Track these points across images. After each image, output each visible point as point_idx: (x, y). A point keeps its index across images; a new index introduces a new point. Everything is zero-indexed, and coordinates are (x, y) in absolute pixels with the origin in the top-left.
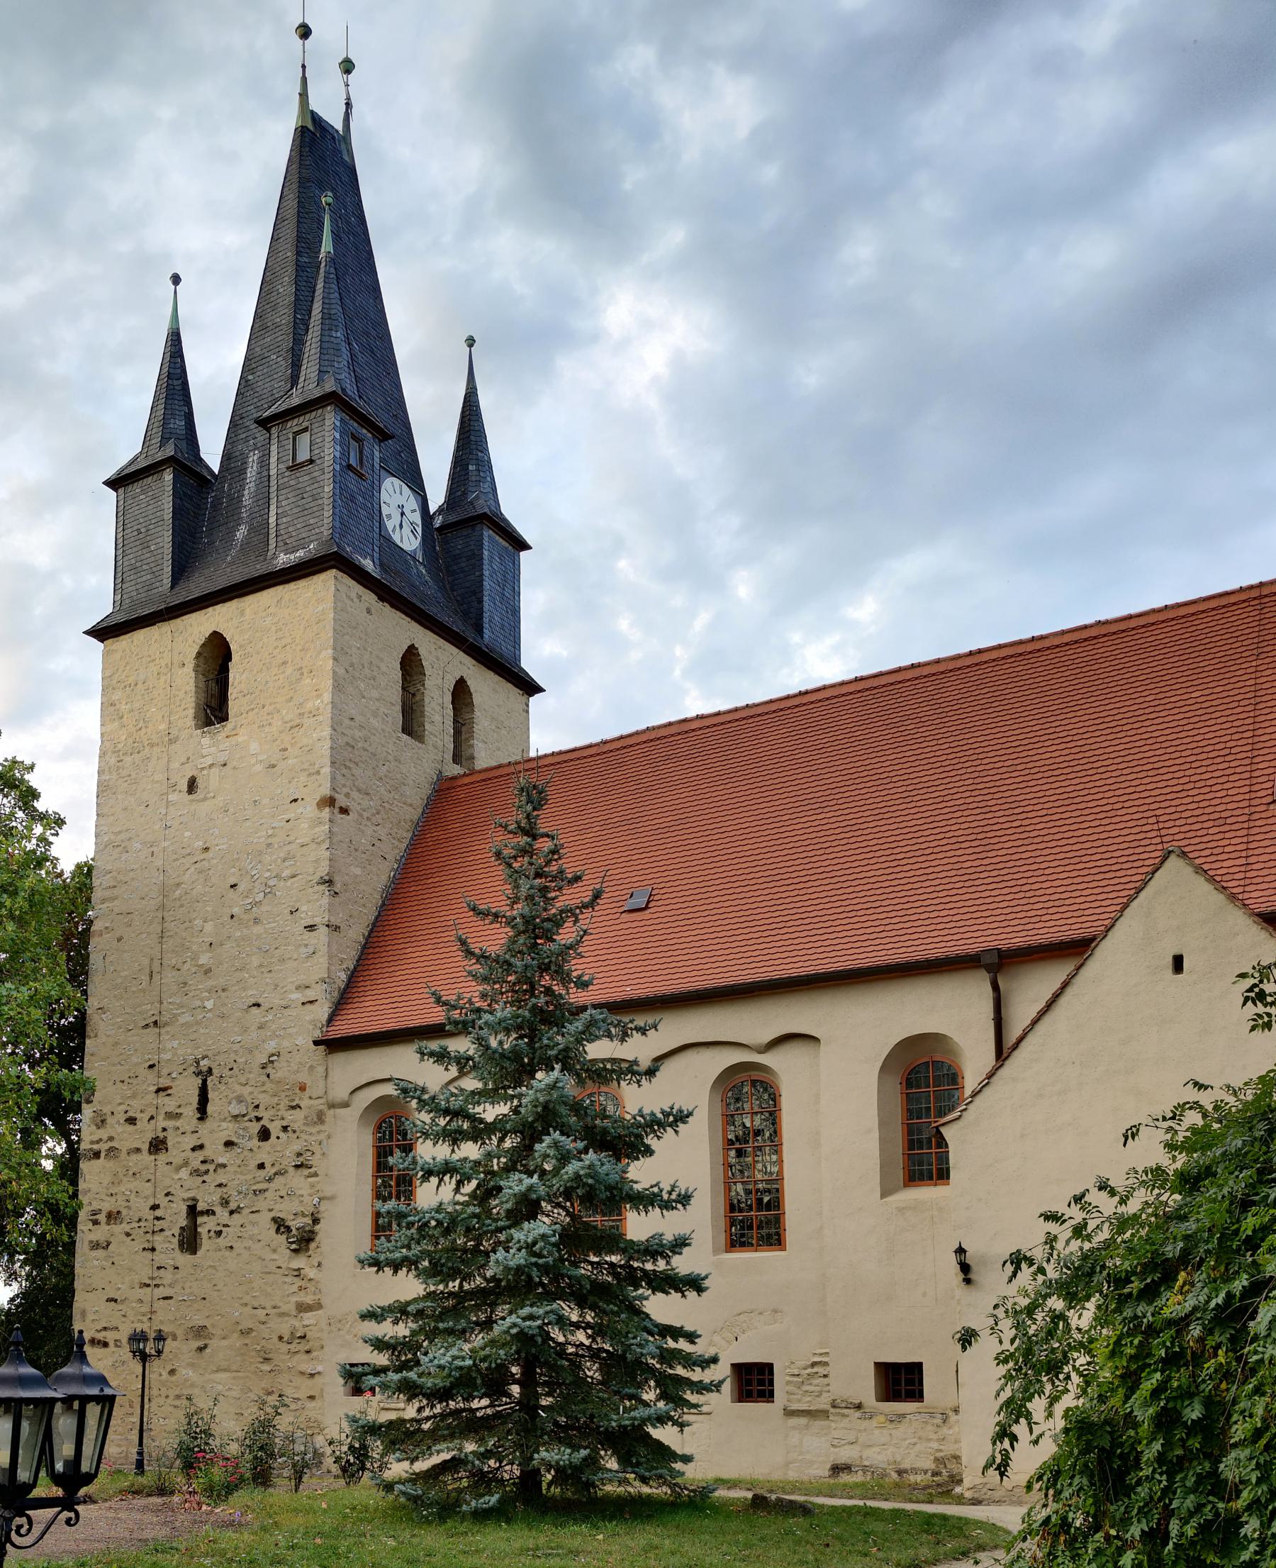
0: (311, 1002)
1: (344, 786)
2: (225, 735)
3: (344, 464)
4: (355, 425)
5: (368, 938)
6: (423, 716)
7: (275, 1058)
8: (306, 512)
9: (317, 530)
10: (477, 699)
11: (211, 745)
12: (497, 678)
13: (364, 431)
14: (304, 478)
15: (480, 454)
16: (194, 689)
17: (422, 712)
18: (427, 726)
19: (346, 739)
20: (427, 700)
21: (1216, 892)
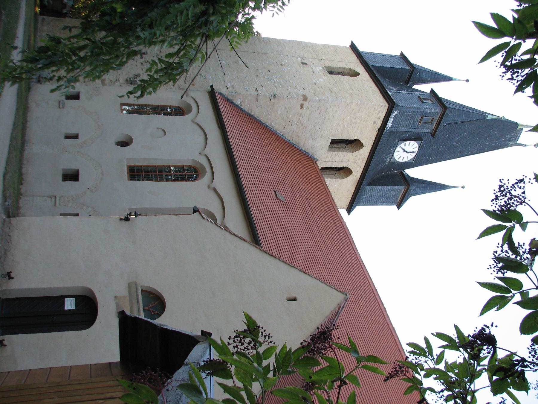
0: (227, 88)
1: (311, 106)
2: (324, 73)
3: (424, 114)
4: (436, 121)
5: (255, 118)
6: (338, 151)
7: (204, 78)
10: (345, 180)
11: (319, 69)
13: (435, 125)
14: (417, 100)
15: (428, 188)
16: (338, 67)
17: (339, 151)
18: (334, 153)
19: (328, 108)
20: (344, 153)
21: (330, 312)
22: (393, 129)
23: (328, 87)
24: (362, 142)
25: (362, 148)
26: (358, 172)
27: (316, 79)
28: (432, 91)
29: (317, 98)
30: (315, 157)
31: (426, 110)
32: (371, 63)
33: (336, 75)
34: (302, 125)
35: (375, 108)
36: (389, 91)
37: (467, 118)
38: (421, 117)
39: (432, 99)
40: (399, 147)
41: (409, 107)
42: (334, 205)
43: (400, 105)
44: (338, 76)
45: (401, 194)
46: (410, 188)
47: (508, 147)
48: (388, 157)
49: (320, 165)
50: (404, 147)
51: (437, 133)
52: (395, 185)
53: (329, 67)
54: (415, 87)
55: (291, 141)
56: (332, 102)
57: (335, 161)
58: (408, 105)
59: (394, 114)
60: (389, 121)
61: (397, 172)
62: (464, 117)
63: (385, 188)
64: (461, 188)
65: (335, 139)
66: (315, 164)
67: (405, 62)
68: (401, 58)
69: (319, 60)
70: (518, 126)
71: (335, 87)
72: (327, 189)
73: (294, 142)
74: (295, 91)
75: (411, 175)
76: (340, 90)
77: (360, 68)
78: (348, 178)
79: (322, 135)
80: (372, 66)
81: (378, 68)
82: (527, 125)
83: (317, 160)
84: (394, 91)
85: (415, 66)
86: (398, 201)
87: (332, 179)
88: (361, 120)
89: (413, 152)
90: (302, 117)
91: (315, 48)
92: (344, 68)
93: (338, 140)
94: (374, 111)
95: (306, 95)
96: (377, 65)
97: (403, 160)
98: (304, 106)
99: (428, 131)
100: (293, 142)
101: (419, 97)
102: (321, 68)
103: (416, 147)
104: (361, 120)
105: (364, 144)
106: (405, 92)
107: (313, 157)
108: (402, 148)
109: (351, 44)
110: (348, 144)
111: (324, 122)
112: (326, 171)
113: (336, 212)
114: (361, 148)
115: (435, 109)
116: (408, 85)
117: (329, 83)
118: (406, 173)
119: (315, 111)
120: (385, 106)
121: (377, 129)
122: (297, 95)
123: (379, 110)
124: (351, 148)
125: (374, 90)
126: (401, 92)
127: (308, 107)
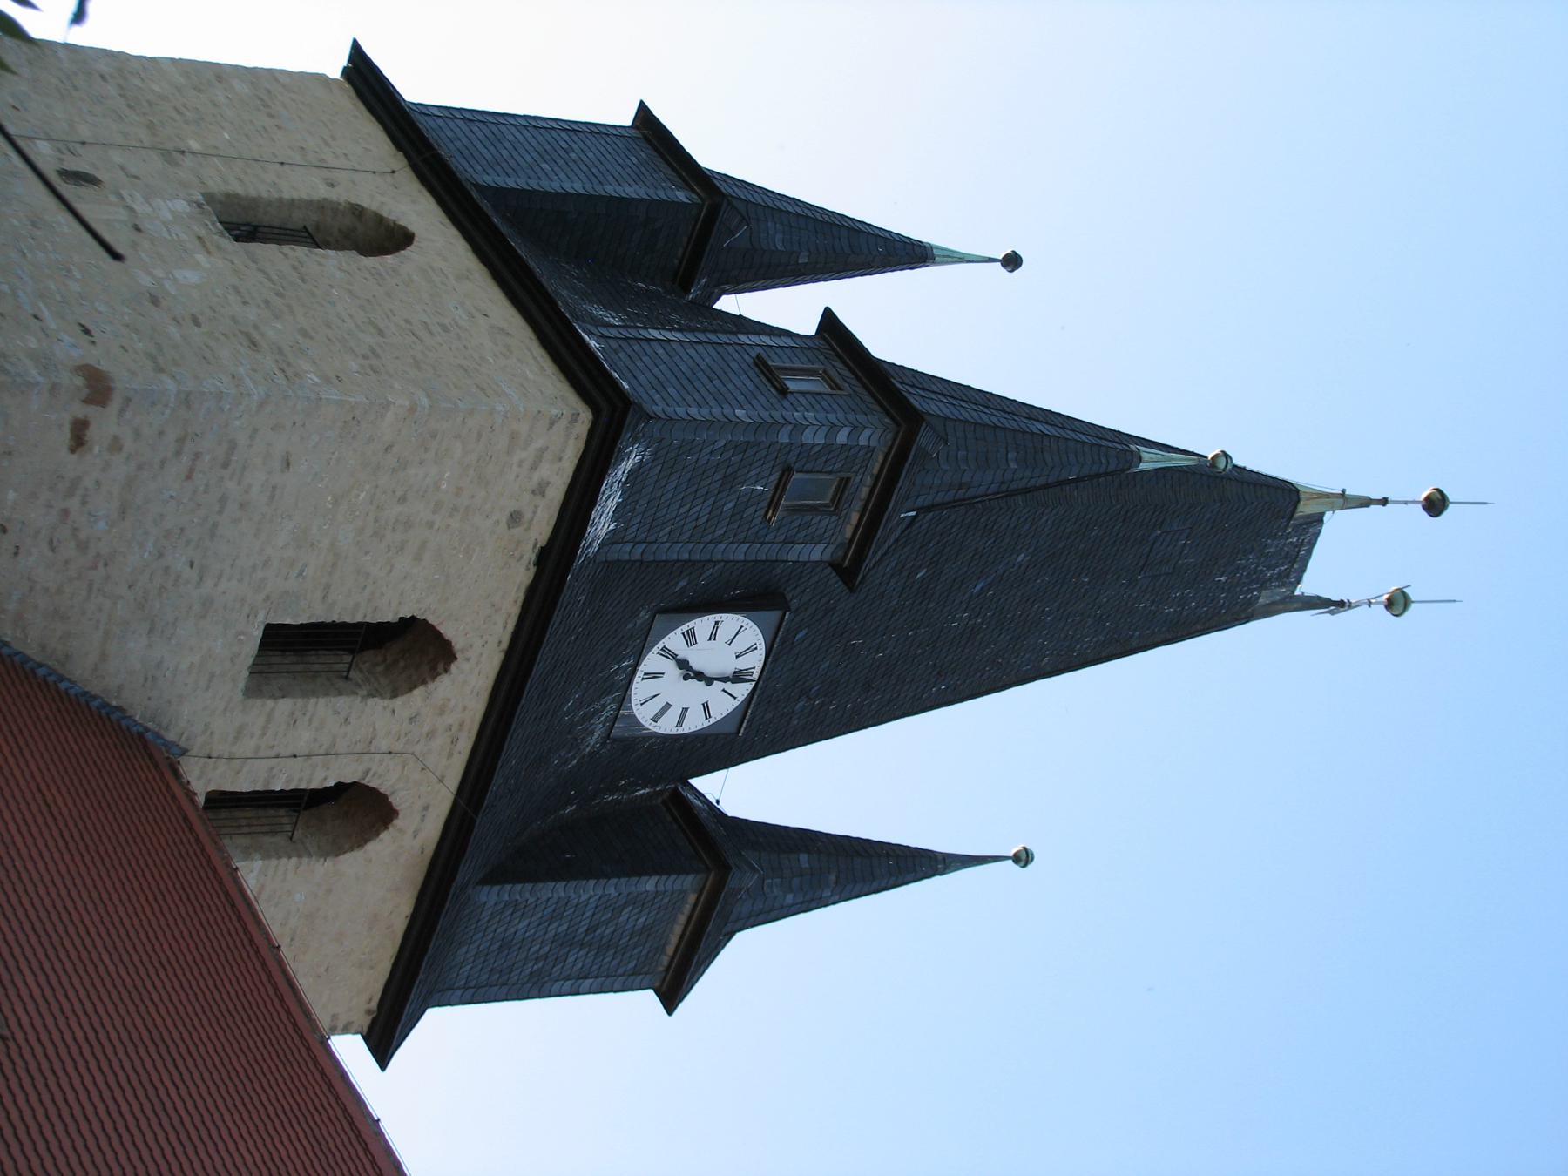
1: (137, 434)
2: (203, 233)
4: (865, 491)
6: (306, 694)
8: (685, 382)
9: (657, 397)
10: (351, 862)
12: (400, 925)
13: (855, 517)
15: (832, 878)
16: (286, 196)
17: (314, 694)
18: (285, 706)
20: (343, 702)
22: (623, 552)
23: (233, 318)
24: (447, 631)
25: (446, 671)
26: (426, 808)
27: (159, 273)
28: (829, 321)
29: (171, 385)
30: (171, 736)
31: (807, 437)
32: (478, 173)
33: (273, 246)
34: (83, 547)
35: (514, 436)
36: (590, 333)
37: (1028, 473)
38: (775, 477)
39: (832, 372)
40: (655, 650)
41: (710, 424)
42: (302, 1022)
43: (658, 409)
44: (286, 248)
45: (682, 919)
46: (732, 883)
47: (1247, 620)
48: (596, 713)
49: (203, 779)
50: (680, 648)
51: (870, 561)
52: (639, 868)
53: (228, 195)
54: (728, 304)
55: (17, 646)
56: (262, 405)
57: (289, 752)
58: (705, 411)
59: (627, 465)
60: (598, 508)
61: (649, 797)
62: (1013, 465)
63: (588, 892)
64: (1010, 862)
65: (288, 621)
66: (169, 776)
67: (664, 166)
68: (644, 145)
69: (166, 155)
70: (1298, 501)
71: (277, 317)
72: (252, 927)
73: (32, 652)
74: (33, 344)
75: (731, 808)
76: (305, 334)
77: (414, 202)
78: (370, 846)
79: (207, 602)
80: (483, 189)
81: (520, 204)
82: (1343, 494)
83: (184, 752)
84: (614, 332)
85: (723, 188)
86: (665, 960)
87: (274, 862)
88: (438, 507)
89: (737, 677)
90: (84, 503)
91: (138, 82)
92: (322, 206)
93: (302, 626)
94: (509, 452)
95: (104, 366)
96: (511, 183)
97: (680, 724)
98: (93, 433)
99: (817, 553)
100: (29, 652)
101: (760, 363)
102: (181, 206)
103: (753, 648)
104: (438, 507)
105: (458, 644)
106: (679, 336)
107: (158, 736)
108: (674, 656)
109: (351, 60)
110: (362, 650)
111: (215, 525)
112: (238, 813)
113: (316, 1063)
114: (440, 667)
115: (856, 429)
116: (687, 291)
117: (238, 292)
118: (700, 795)
119: (163, 462)
120: (575, 418)
121: (530, 555)
122: (45, 362)
123: (539, 443)
124: (380, 669)
125: (501, 330)
126: (655, 334)
127: (116, 439)
